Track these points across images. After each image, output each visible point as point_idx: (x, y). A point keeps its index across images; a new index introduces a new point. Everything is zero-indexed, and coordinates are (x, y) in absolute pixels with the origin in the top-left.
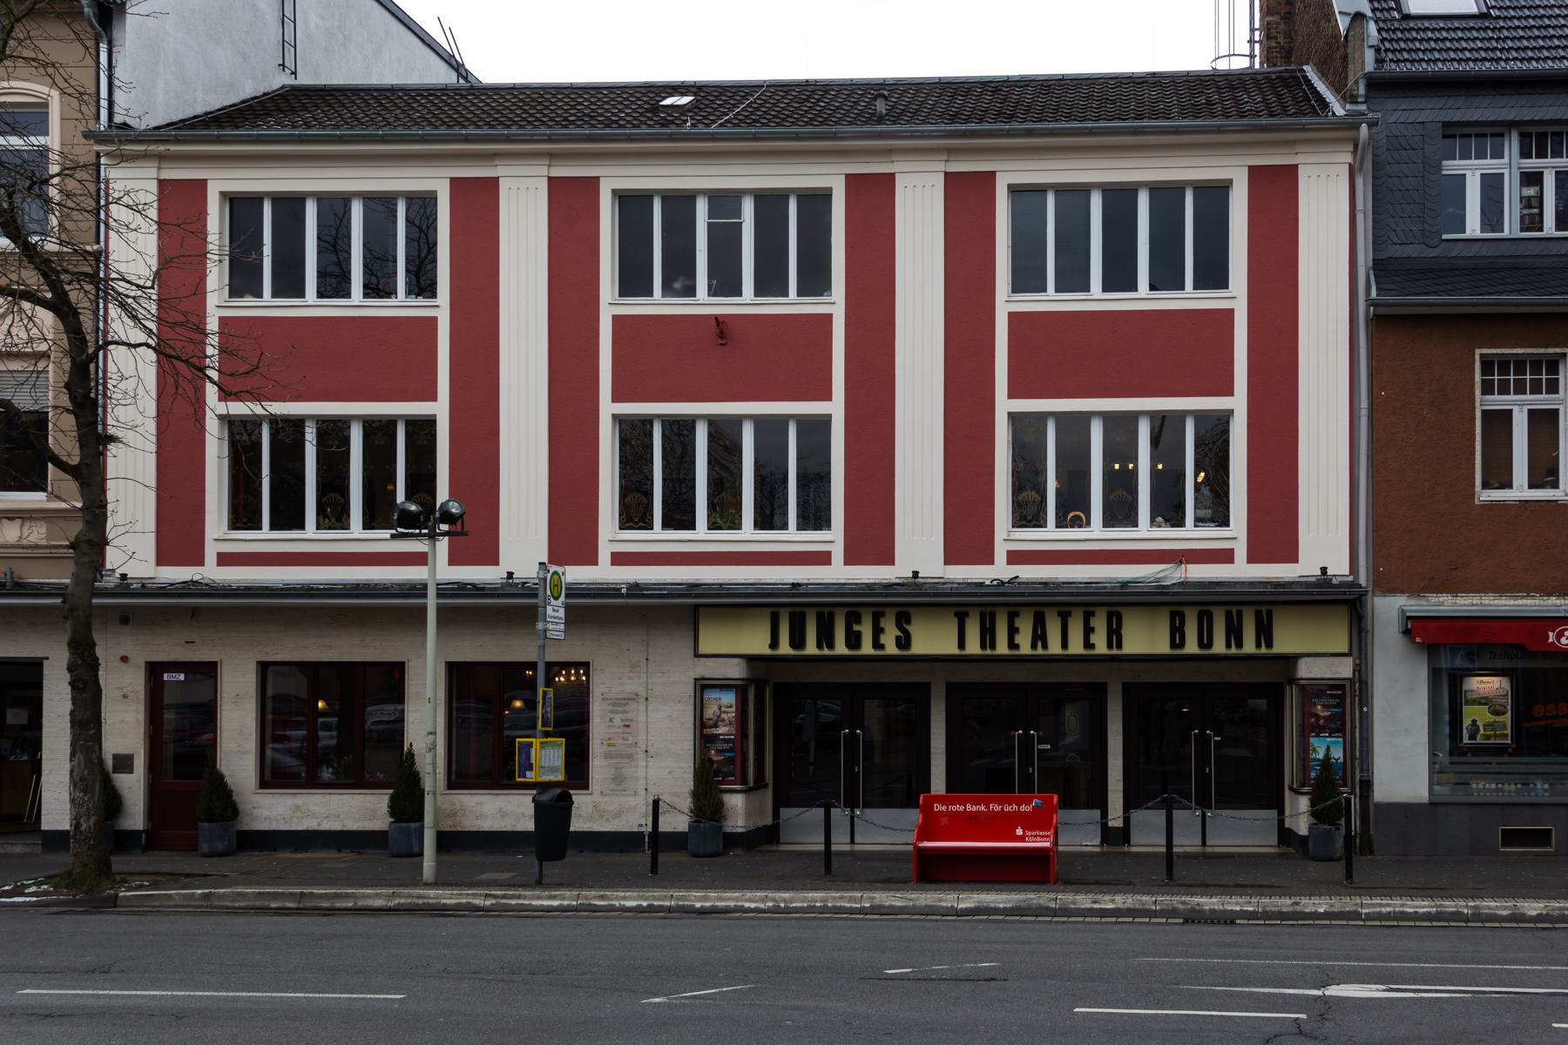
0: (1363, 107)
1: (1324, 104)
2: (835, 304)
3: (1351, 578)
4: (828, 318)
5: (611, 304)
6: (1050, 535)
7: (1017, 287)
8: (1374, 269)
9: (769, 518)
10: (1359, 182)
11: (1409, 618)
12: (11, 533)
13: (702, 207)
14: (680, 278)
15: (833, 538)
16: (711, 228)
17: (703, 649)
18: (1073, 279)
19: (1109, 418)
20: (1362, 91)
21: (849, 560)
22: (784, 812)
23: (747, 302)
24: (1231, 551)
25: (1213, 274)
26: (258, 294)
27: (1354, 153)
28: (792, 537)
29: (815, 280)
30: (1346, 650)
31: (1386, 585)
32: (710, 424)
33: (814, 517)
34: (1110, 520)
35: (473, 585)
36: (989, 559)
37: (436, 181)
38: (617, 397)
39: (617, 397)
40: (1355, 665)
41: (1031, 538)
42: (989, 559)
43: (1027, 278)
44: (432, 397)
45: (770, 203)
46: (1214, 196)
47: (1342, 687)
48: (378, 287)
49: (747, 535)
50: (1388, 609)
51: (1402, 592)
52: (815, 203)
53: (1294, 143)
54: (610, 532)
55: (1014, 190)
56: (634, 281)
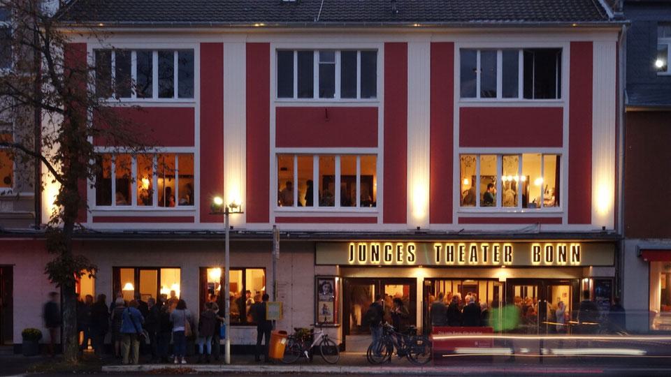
0: (621, 14)
1: (604, 11)
2: (378, 102)
3: (615, 231)
4: (376, 109)
5: (275, 102)
6: (294, 210)
7: (280, 94)
8: (627, 89)
9: (347, 201)
10: (620, 50)
11: (641, 250)
12: (7, 208)
13: (316, 57)
14: (306, 92)
15: (378, 211)
16: (321, 66)
17: (317, 263)
18: (306, 92)
19: (322, 157)
20: (621, 6)
21: (386, 221)
22: (347, 337)
23: (337, 100)
24: (561, 218)
25: (369, 91)
26: (291, 96)
27: (619, 37)
28: (358, 210)
29: (187, 92)
30: (612, 264)
31: (630, 234)
32: (321, 160)
33: (368, 201)
34: (322, 203)
35: (251, 232)
36: (450, 221)
37: (193, 44)
38: (278, 145)
39: (278, 145)
40: (616, 271)
41: (285, 210)
42: (450, 221)
43: (468, 92)
44: (192, 144)
45: (348, 56)
46: (369, 56)
47: (610, 281)
48: (166, 93)
49: (338, 209)
50: (632, 246)
51: (638, 238)
52: (186, 57)
53: (406, 33)
54: (276, 209)
55: (462, 50)
56: (285, 91)
